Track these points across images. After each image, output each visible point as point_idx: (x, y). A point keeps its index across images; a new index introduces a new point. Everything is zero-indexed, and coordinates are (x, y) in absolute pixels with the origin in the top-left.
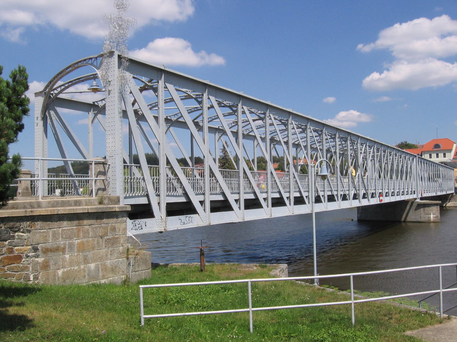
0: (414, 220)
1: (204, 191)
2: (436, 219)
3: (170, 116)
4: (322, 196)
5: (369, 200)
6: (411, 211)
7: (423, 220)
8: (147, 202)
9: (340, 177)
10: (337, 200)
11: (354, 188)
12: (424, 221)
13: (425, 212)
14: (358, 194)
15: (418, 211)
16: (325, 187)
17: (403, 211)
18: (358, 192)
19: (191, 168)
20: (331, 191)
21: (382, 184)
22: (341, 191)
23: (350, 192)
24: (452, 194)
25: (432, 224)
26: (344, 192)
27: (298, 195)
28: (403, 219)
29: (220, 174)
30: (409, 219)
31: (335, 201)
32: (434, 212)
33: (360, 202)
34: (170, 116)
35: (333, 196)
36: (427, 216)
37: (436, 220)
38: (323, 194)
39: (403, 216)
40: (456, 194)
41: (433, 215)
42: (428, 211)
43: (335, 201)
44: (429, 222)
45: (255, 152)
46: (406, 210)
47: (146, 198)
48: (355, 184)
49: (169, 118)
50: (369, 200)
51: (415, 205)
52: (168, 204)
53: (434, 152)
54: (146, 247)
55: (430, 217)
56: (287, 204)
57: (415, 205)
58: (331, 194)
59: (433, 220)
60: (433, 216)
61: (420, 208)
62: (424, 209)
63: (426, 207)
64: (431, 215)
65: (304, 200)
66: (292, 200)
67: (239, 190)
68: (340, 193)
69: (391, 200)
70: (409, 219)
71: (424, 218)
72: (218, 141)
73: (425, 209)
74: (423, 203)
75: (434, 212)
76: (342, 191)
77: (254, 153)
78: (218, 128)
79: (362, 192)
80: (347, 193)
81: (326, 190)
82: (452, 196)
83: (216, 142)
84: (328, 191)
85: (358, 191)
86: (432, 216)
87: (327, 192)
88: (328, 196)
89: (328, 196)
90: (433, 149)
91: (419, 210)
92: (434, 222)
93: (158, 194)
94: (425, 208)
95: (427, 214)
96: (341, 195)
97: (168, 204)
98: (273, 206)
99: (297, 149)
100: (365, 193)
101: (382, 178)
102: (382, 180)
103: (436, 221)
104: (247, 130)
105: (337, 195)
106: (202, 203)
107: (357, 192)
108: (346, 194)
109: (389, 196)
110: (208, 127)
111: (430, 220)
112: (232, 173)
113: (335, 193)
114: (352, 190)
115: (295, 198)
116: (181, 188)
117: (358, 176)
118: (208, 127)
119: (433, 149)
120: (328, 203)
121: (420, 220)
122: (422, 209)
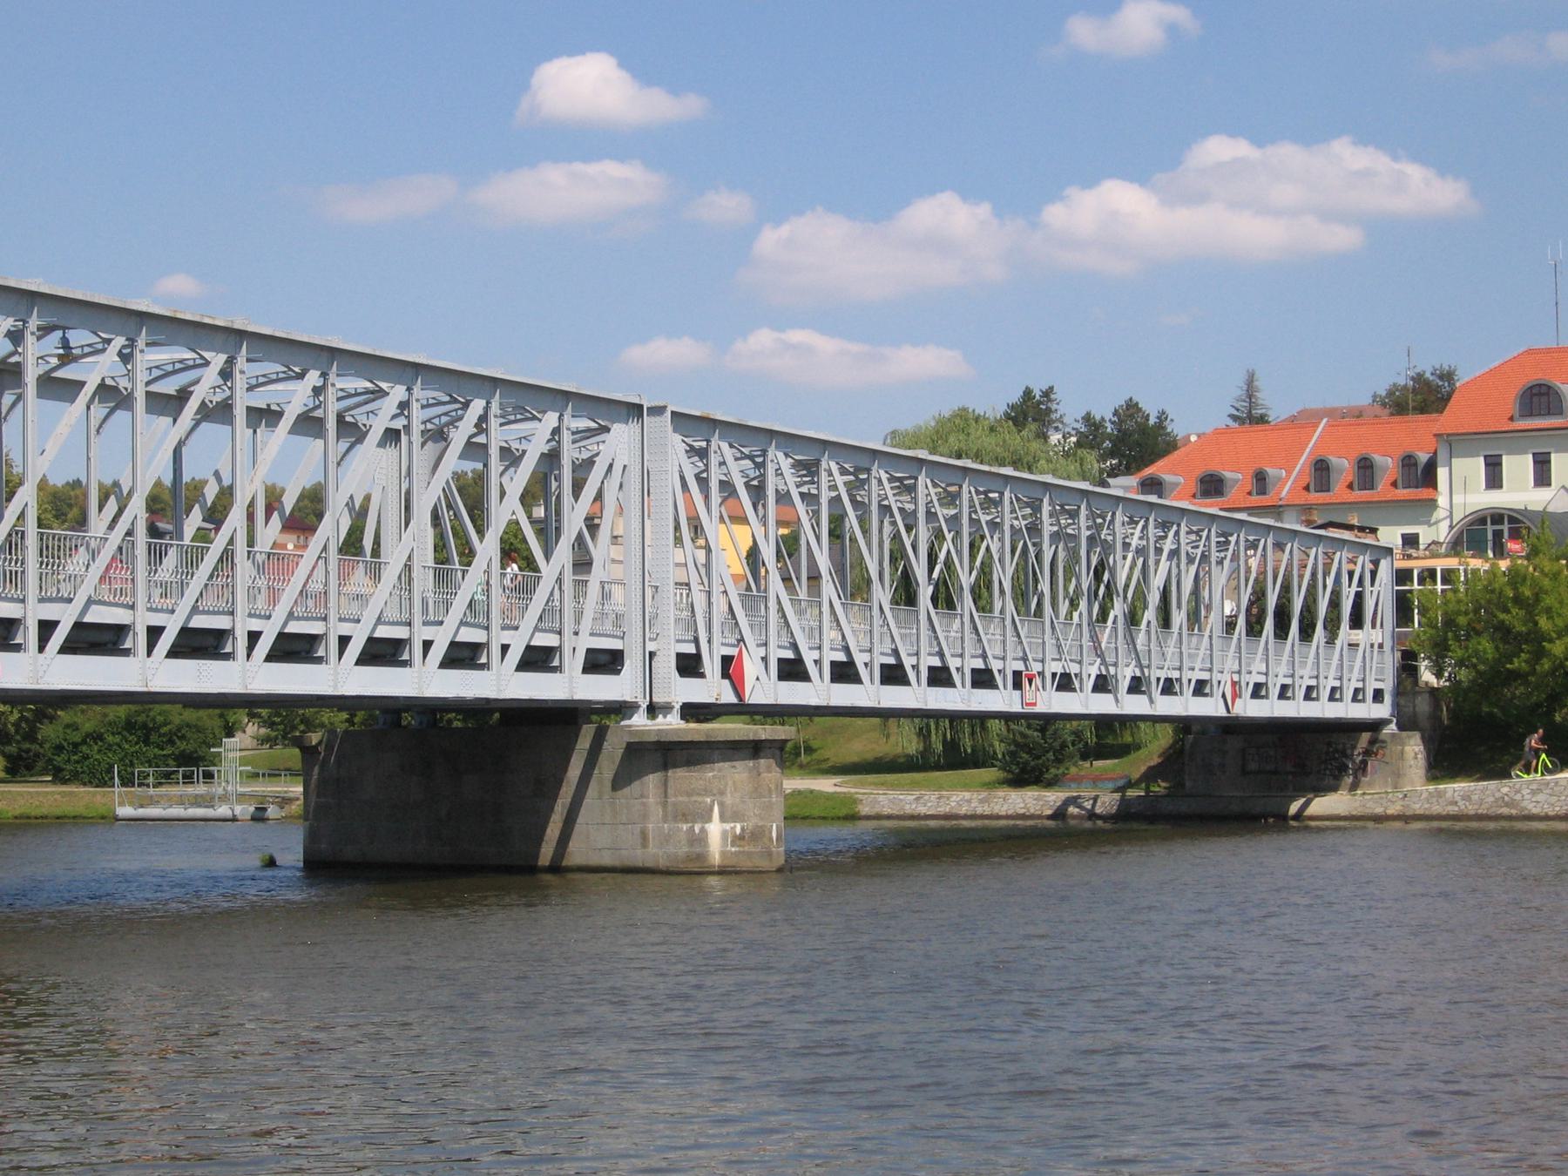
0: (607, 859)
1: (233, 604)
2: (746, 849)
3: (113, 378)
4: (999, 671)
5: (1151, 701)
6: (592, 791)
7: (654, 854)
8: (694, 651)
9: (1052, 622)
10: (1078, 690)
11: (1099, 656)
12: (663, 863)
13: (671, 800)
14: (1145, 678)
15: (626, 791)
16: (966, 645)
17: (548, 787)
18: (1147, 674)
19: (368, 559)
20: (1025, 659)
21: (1318, 658)
22: (1158, 668)
23: (1084, 667)
24: (1375, 726)
25: (713, 881)
26: (1063, 667)
27: (936, 662)
28: (546, 854)
29: (789, 603)
30: (577, 853)
31: (1074, 690)
32: (728, 800)
33: (1117, 700)
34: (113, 378)
35: (945, 669)
36: (685, 827)
37: (749, 854)
38: (1001, 667)
39: (549, 831)
40: (1401, 727)
41: (723, 819)
42: (689, 794)
43: (907, 683)
44: (692, 871)
45: (91, 455)
46: (564, 789)
47: (693, 645)
48: (1103, 645)
49: (109, 382)
50: (1151, 701)
51: (613, 748)
52: (589, 651)
53: (1515, 439)
54: (157, 708)
55: (703, 830)
56: (864, 680)
57: (613, 748)
58: (983, 667)
59: (723, 854)
60: (728, 826)
61: (640, 775)
62: (665, 784)
63: (675, 766)
64: (709, 820)
65: (905, 675)
66: (924, 674)
67: (488, 620)
68: (774, 653)
69: (929, 703)
70: (577, 853)
71: (666, 839)
72: (98, 431)
73: (671, 783)
74: (653, 738)
75: (728, 800)
76: (1162, 668)
77: (88, 459)
78: (265, 407)
79: (1127, 673)
80: (1074, 669)
81: (1009, 656)
82: (1372, 742)
83: (93, 436)
84: (1014, 659)
85: (1146, 670)
86: (715, 830)
87: (335, 624)
88: (973, 671)
89: (973, 671)
90: (1511, 419)
91: (636, 785)
92: (722, 872)
93: (21, 597)
94: (670, 773)
95: (685, 817)
96: (1054, 675)
97: (589, 651)
98: (833, 680)
99: (255, 432)
100: (1139, 678)
101: (1240, 634)
102: (1267, 643)
103: (746, 864)
104: (217, 390)
105: (915, 667)
106: (915, 667)
107: (1107, 670)
108: (1070, 674)
109: (1294, 699)
110: (247, 407)
111: (702, 857)
112: (48, 539)
113: (995, 665)
114: (1127, 666)
115: (931, 669)
116: (757, 632)
117: (1114, 623)
118: (247, 407)
119: (1511, 419)
120: (975, 690)
121: (638, 857)
122: (652, 781)
